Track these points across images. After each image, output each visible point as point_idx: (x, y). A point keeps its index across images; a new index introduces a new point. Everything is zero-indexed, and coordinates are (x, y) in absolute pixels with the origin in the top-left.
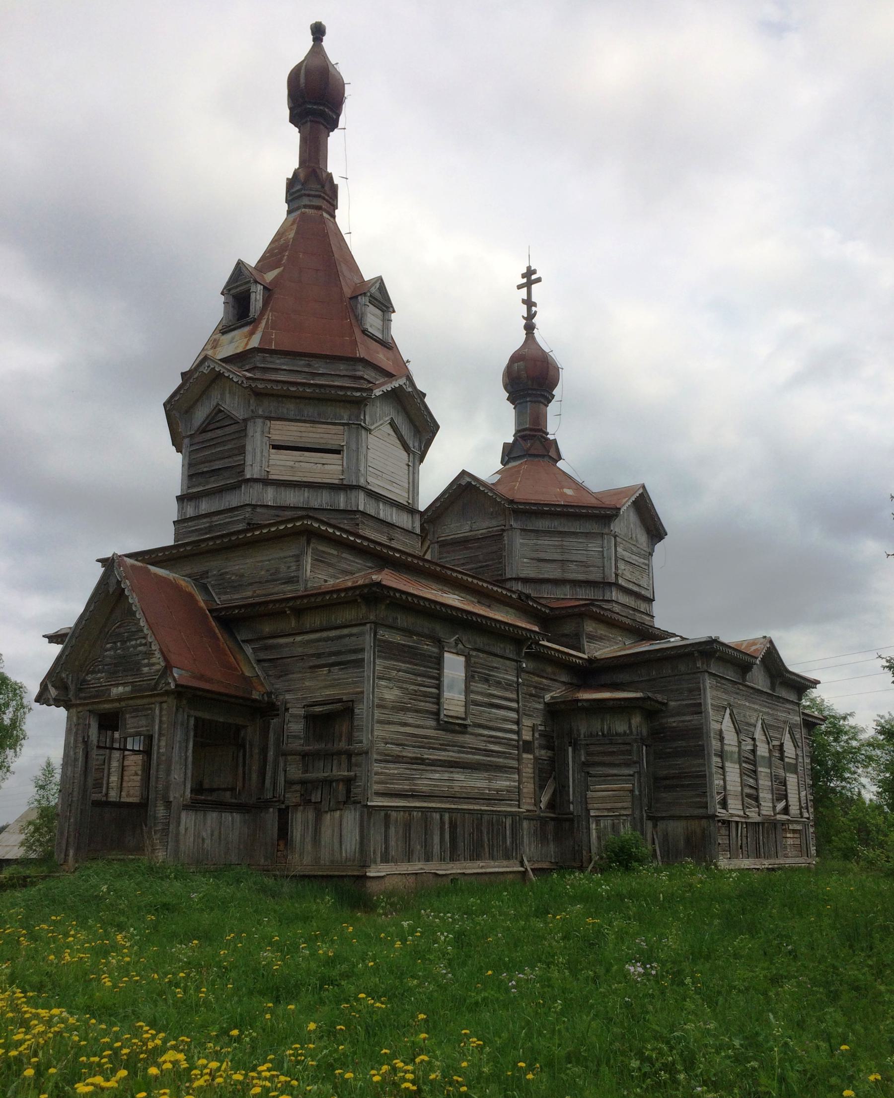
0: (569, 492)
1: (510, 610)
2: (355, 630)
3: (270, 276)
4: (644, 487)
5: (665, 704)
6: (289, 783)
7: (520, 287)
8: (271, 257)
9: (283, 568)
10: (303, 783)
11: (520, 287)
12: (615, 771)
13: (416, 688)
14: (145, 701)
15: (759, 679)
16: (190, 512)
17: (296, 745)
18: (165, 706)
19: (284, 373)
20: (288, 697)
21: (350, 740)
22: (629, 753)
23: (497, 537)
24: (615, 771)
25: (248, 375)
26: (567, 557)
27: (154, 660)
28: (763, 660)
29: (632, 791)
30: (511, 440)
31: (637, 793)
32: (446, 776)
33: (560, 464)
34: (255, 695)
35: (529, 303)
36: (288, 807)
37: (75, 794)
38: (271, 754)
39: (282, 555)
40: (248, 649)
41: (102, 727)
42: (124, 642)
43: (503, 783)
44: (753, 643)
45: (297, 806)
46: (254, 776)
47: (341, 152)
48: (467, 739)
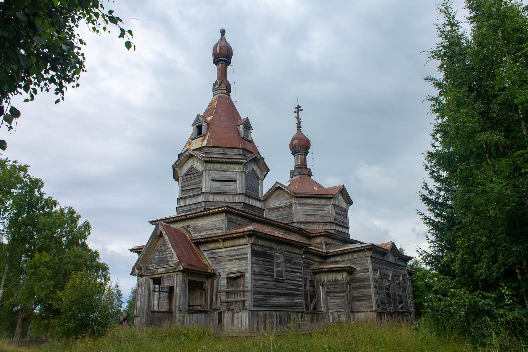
0: (316, 189)
1: (297, 235)
2: (244, 247)
3: (209, 119)
4: (343, 186)
5: (355, 269)
6: (222, 303)
7: (295, 112)
8: (208, 112)
9: (217, 224)
10: (227, 302)
11: (295, 112)
12: (338, 295)
13: (266, 267)
14: (171, 274)
15: (391, 258)
16: (182, 204)
17: (224, 288)
18: (178, 276)
19: (216, 153)
20: (221, 271)
21: (244, 287)
22: (343, 287)
23: (290, 206)
24: (338, 295)
25: (204, 155)
26: (316, 213)
27: (174, 259)
28: (391, 250)
29: (344, 302)
30: (293, 169)
31: (346, 302)
32: (277, 299)
33: (312, 177)
34: (209, 271)
35: (298, 118)
36: (221, 312)
37: (145, 308)
38: (215, 292)
39: (217, 219)
40: (205, 254)
41: (154, 283)
42: (162, 253)
43: (297, 301)
44: (387, 244)
45: (225, 311)
46: (209, 301)
47: (233, 73)
48: (284, 285)
